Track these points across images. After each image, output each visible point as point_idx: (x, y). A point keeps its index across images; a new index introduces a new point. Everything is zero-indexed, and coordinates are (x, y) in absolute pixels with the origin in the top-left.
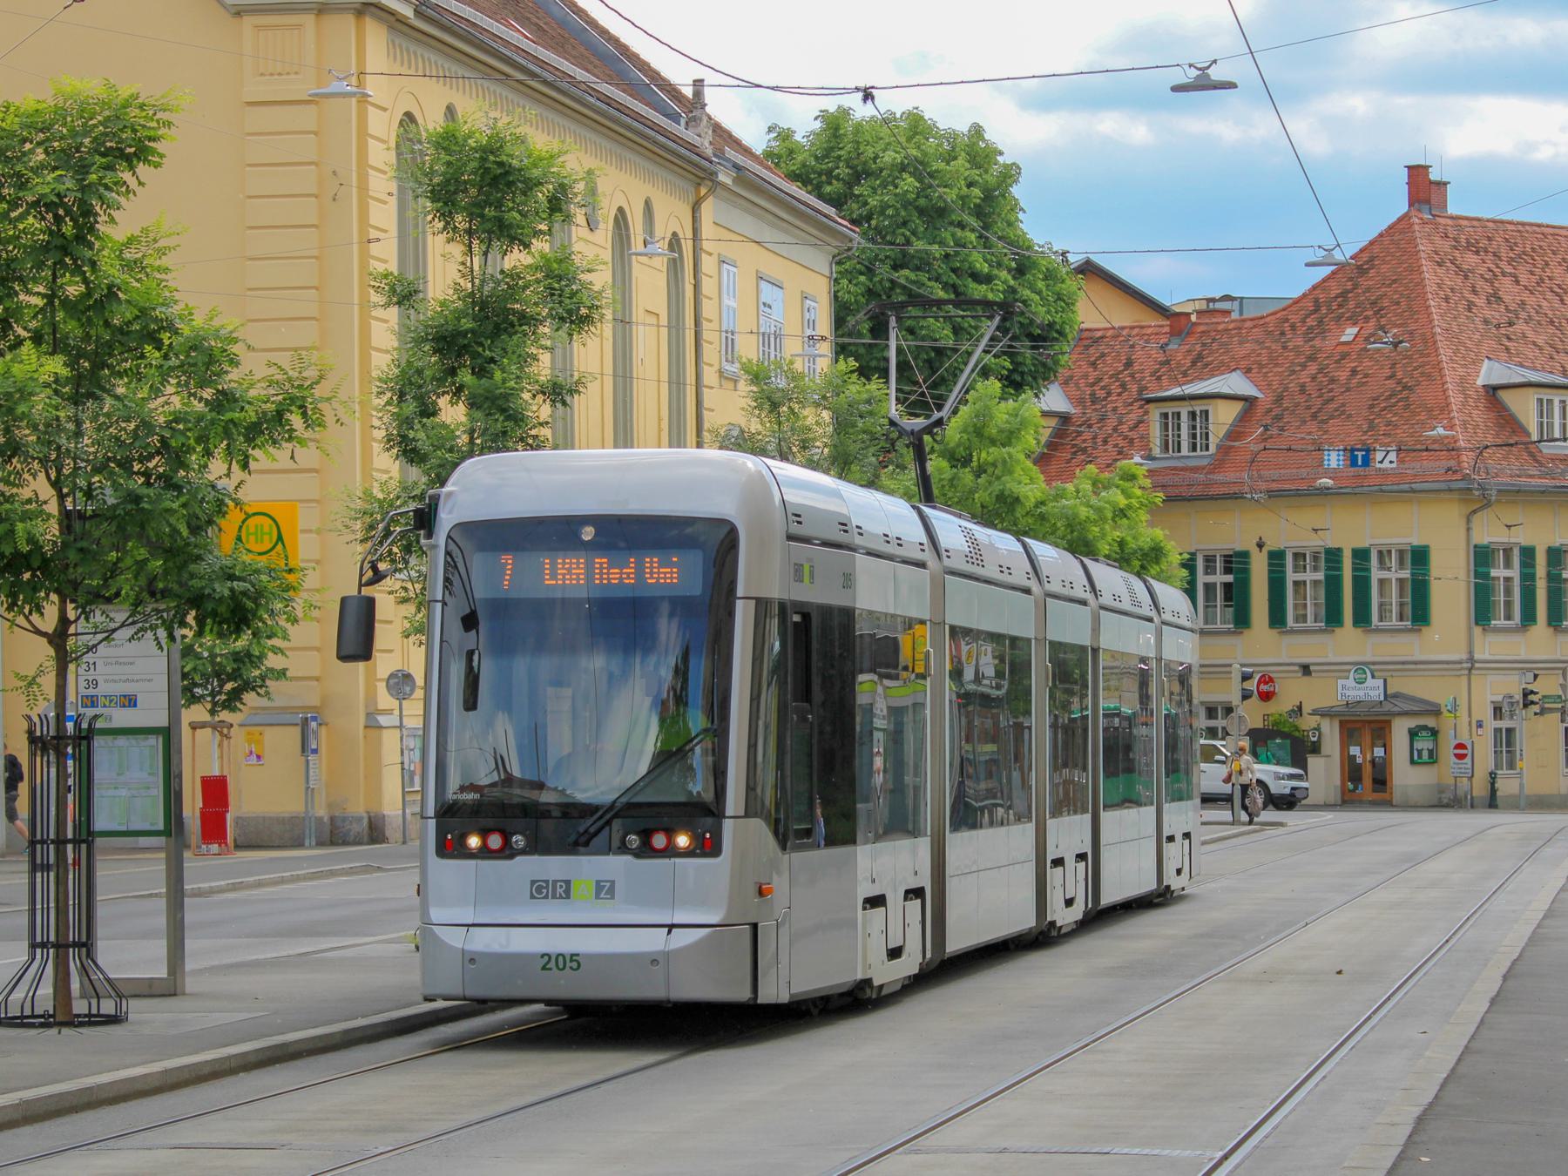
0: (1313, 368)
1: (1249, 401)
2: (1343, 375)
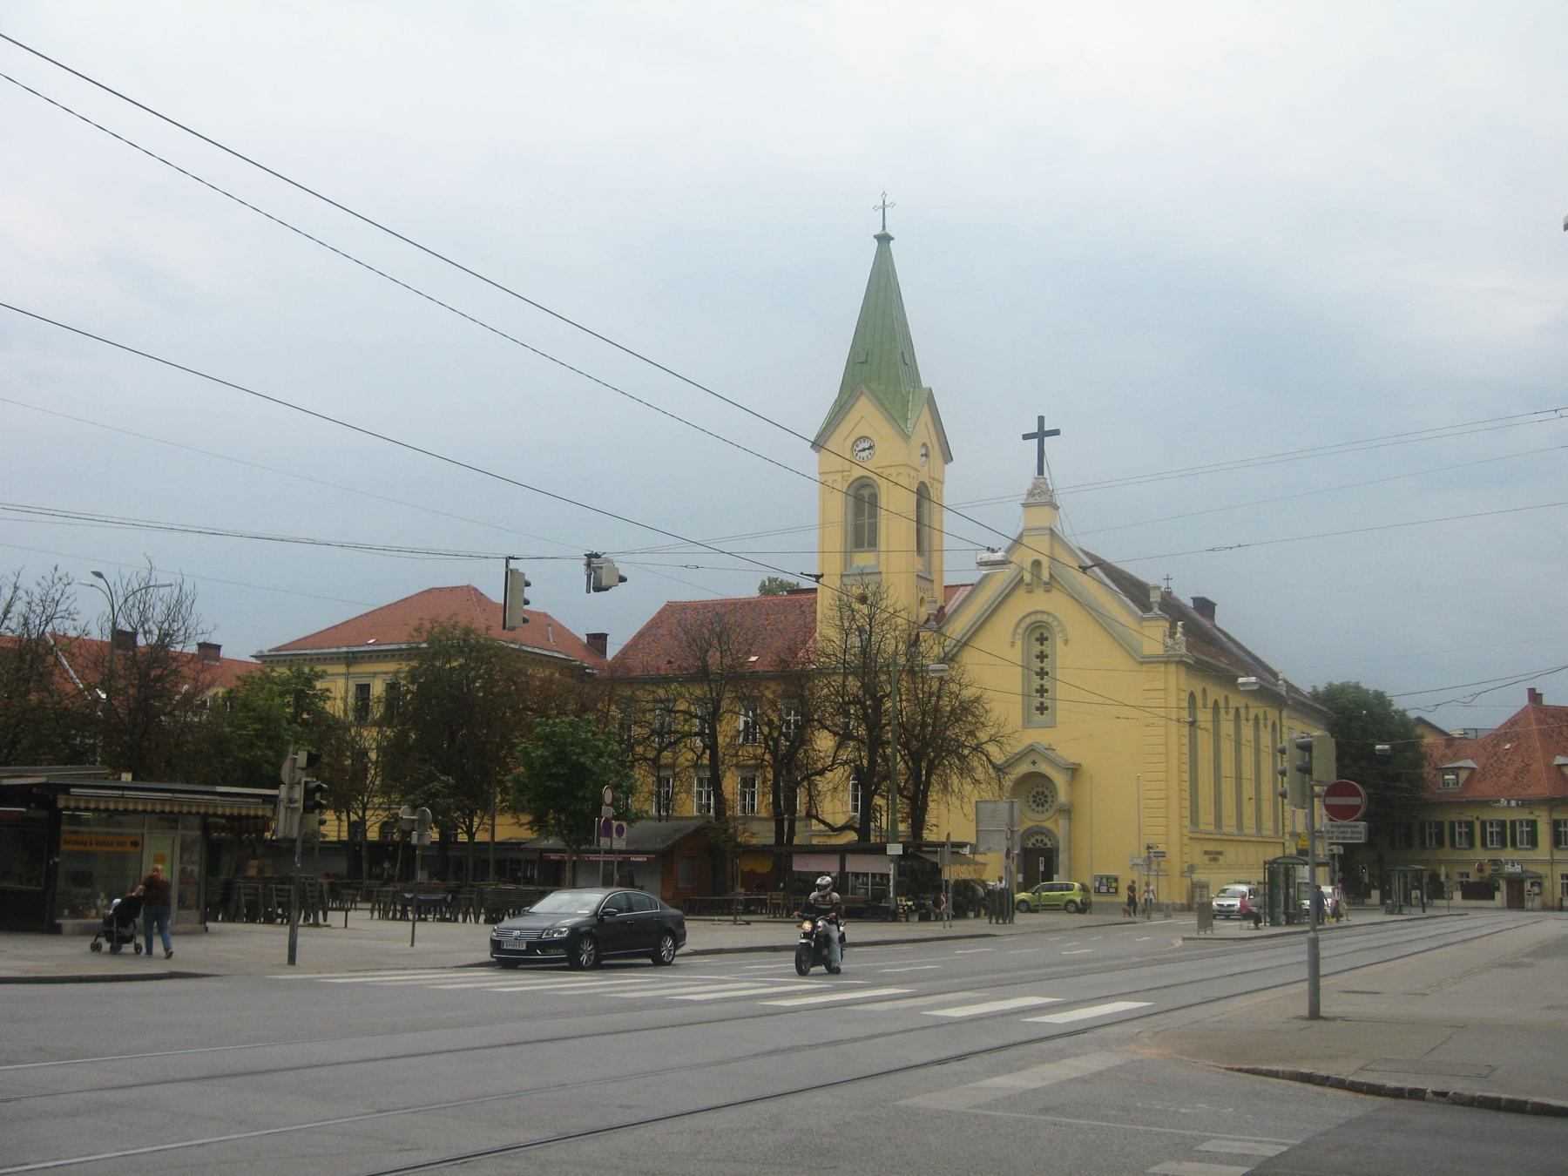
0: (1495, 758)
1: (1474, 769)
2: (1506, 760)
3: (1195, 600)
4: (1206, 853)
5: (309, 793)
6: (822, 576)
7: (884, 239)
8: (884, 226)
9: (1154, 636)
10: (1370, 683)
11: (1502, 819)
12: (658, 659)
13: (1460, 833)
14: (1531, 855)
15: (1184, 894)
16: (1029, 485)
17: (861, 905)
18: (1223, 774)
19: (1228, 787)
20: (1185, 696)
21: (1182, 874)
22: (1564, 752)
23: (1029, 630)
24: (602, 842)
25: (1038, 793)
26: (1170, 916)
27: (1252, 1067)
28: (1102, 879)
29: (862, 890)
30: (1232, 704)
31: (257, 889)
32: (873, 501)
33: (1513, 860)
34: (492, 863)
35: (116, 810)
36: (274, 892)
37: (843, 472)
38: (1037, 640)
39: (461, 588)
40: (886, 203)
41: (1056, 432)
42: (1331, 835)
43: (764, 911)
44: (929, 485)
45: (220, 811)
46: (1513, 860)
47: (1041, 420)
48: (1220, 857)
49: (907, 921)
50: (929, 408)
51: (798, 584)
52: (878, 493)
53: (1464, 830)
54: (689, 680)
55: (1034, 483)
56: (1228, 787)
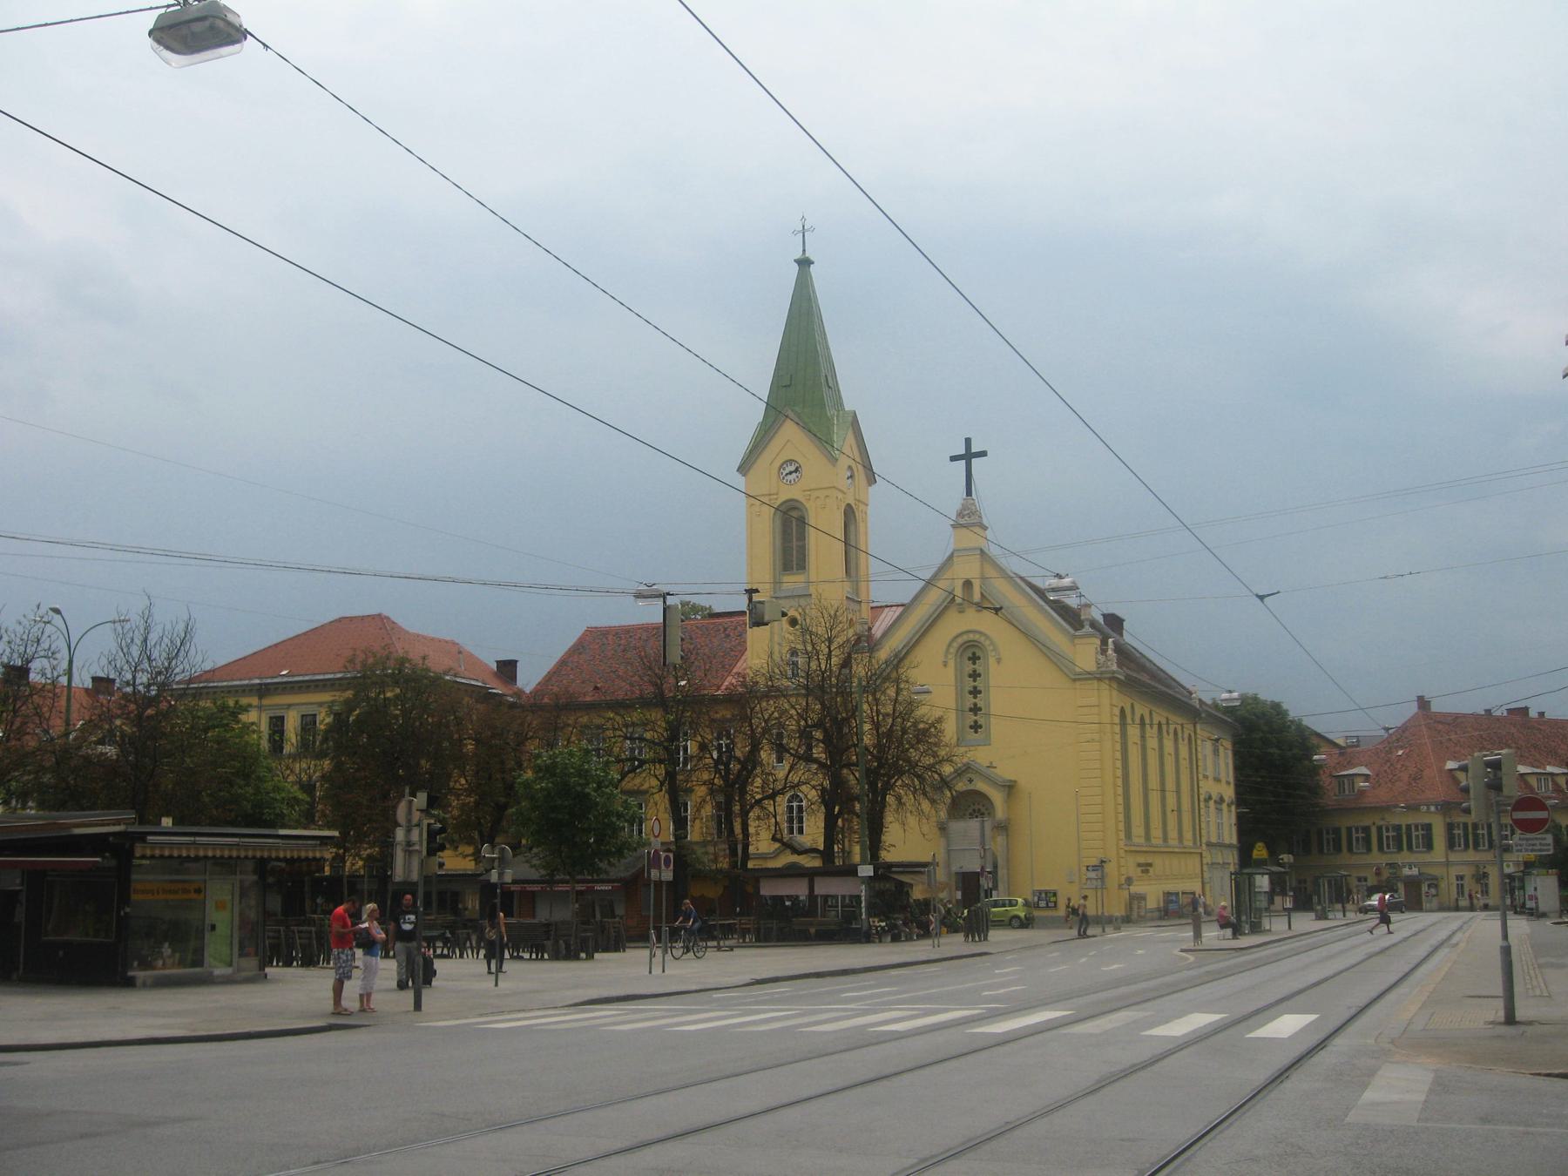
0: (1389, 764)
2: (1399, 766)
3: (1104, 616)
4: (1139, 865)
5: (432, 834)
6: (1001, 608)
7: (804, 263)
8: (804, 251)
9: (1086, 654)
10: (1266, 695)
11: (1397, 823)
12: (584, 685)
13: (1357, 839)
14: (1427, 858)
15: (1123, 907)
16: (959, 507)
17: (833, 927)
18: (1150, 787)
19: (1155, 798)
20: (1117, 711)
21: (1120, 886)
22: (1455, 757)
23: (962, 649)
24: (652, 874)
25: (974, 810)
26: (1119, 929)
27: (1548, 1072)
28: (1040, 894)
29: (833, 913)
30: (1156, 719)
31: (279, 931)
32: (802, 522)
33: (1410, 863)
34: (366, 892)
35: (188, 857)
36: (297, 934)
37: (770, 495)
38: (969, 659)
39: (373, 617)
40: (806, 228)
41: (983, 454)
42: (1519, 848)
43: (977, 939)
44: (854, 506)
45: (281, 855)
46: (1410, 863)
47: (968, 441)
48: (1151, 870)
49: (880, 942)
50: (854, 433)
51: (710, 607)
52: (806, 514)
53: (1361, 835)
54: (646, 703)
55: (963, 505)
56: (1155, 798)
